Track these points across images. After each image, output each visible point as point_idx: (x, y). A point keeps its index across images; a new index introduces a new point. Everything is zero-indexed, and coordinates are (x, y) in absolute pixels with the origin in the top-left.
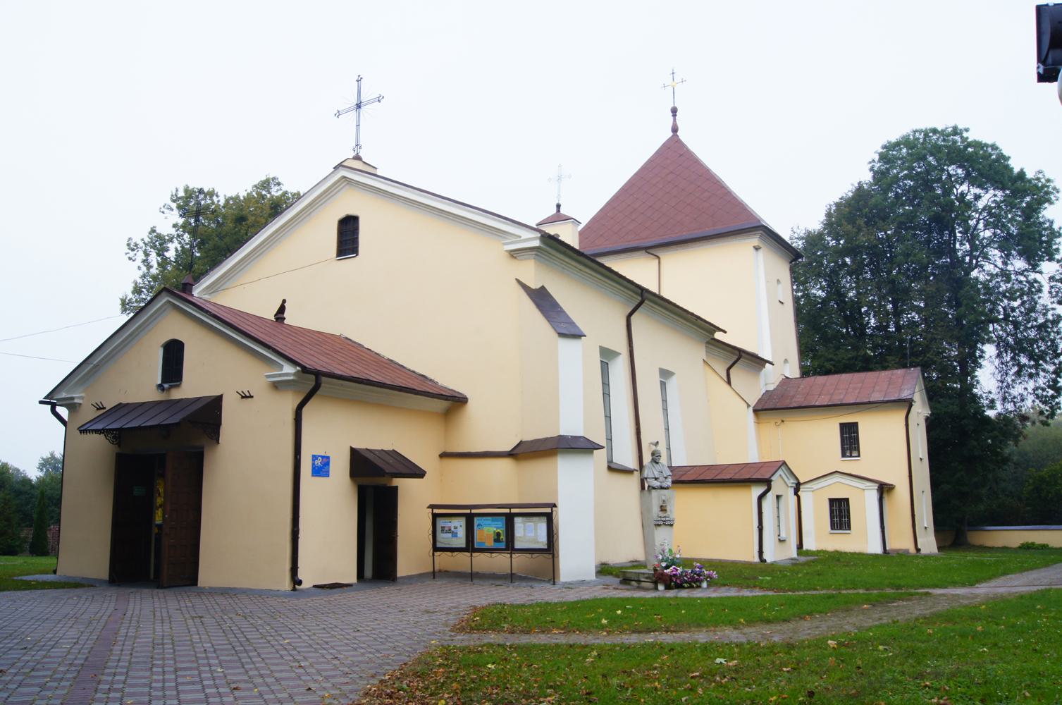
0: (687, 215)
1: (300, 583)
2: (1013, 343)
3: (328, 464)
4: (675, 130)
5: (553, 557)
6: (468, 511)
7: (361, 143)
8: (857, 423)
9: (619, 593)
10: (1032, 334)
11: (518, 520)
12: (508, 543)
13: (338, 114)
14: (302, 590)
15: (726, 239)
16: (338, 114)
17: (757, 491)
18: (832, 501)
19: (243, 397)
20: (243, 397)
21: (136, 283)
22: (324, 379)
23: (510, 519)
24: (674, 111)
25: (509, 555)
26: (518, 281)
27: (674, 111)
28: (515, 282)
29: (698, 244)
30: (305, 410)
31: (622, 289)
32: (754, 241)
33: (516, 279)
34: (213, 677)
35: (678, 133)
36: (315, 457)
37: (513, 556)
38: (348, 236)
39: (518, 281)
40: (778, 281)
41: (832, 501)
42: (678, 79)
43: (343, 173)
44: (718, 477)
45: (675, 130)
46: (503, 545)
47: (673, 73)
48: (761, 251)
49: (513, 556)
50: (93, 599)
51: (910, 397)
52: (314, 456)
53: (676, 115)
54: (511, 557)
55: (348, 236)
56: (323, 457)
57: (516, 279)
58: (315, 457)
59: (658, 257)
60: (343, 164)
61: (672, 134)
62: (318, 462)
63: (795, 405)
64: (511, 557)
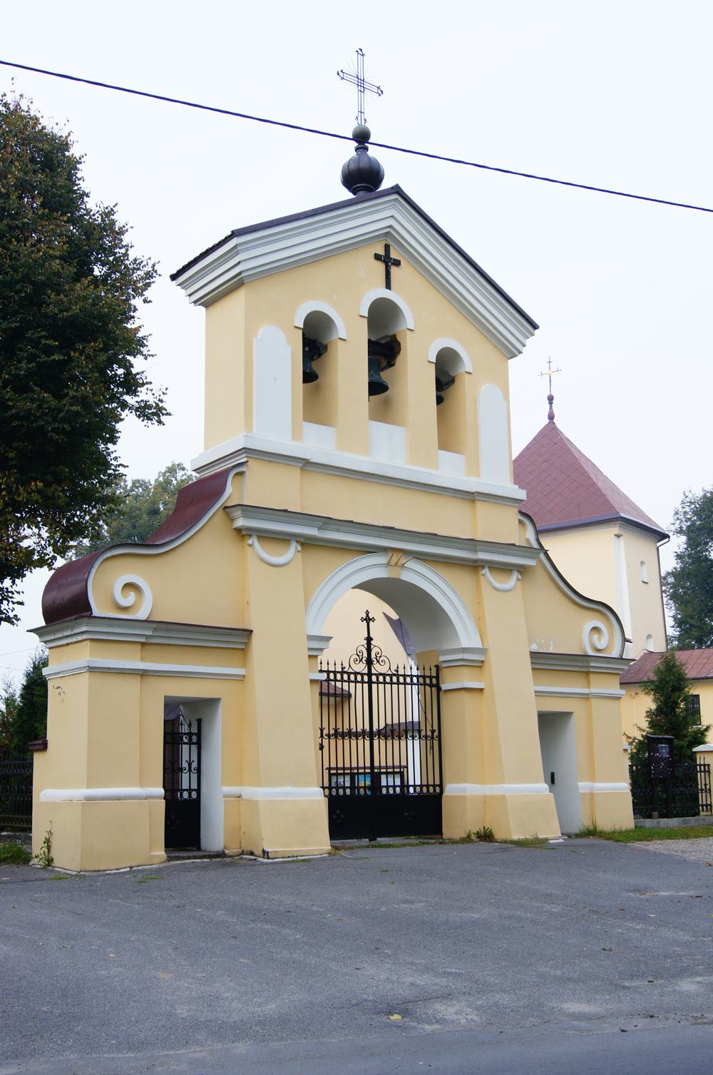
0: (557, 505)
4: (551, 417)
8: (698, 696)
10: (187, 993)
13: (360, 52)
15: (590, 528)
16: (360, 52)
21: (118, 432)
24: (551, 399)
26: (384, 614)
27: (551, 399)
28: (383, 615)
29: (566, 532)
32: (615, 529)
34: (370, 674)
35: (555, 421)
39: (384, 614)
40: (642, 563)
42: (554, 368)
45: (551, 417)
48: (622, 538)
50: (147, 383)
53: (552, 403)
61: (548, 421)
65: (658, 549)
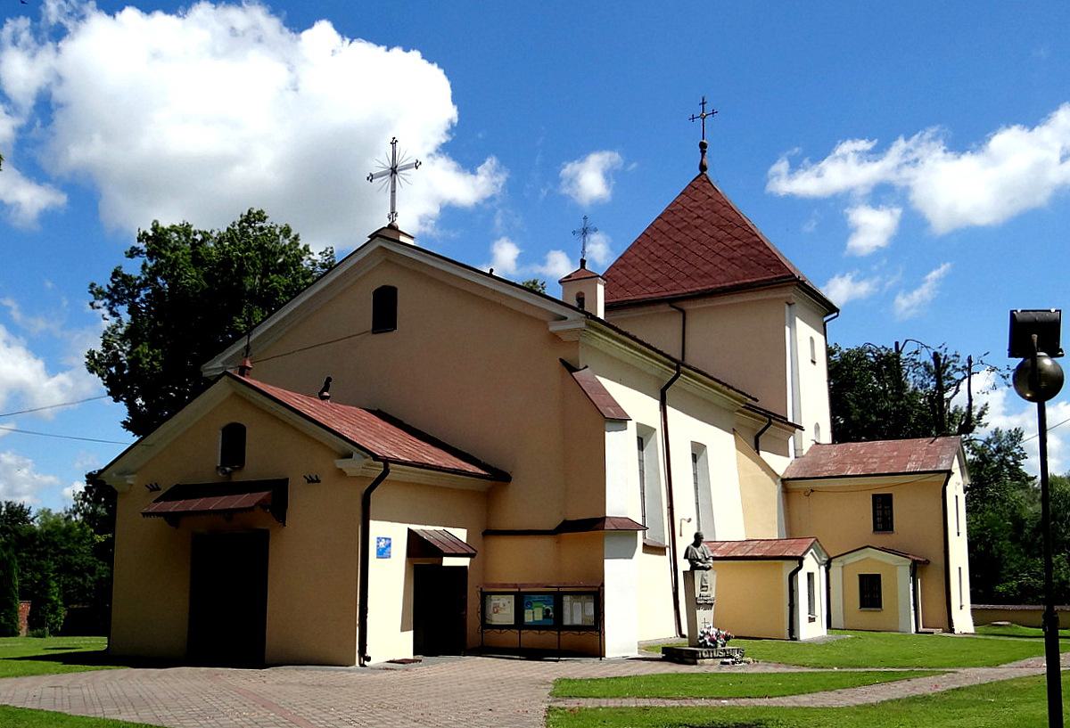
1: (369, 659)
2: (948, 264)
3: (390, 545)
4: (703, 168)
5: (600, 633)
6: (556, 590)
7: (396, 210)
9: (666, 668)
11: (567, 599)
12: (555, 620)
14: (372, 668)
17: (789, 567)
18: (862, 577)
19: (309, 482)
20: (309, 482)
22: (391, 465)
23: (557, 598)
24: (703, 146)
25: (517, 631)
30: (373, 495)
31: (628, 349)
33: (561, 360)
36: (379, 539)
37: (561, 633)
38: (385, 311)
41: (862, 577)
42: (708, 109)
43: (378, 243)
44: (749, 554)
45: (703, 168)
46: (550, 622)
47: (703, 103)
49: (561, 633)
51: (949, 468)
52: (378, 538)
54: (559, 634)
55: (385, 311)
56: (386, 539)
57: (561, 360)
58: (379, 539)
59: (684, 313)
60: (379, 233)
61: (699, 172)
62: (382, 544)
63: (826, 474)
64: (559, 634)
65: (825, 325)
